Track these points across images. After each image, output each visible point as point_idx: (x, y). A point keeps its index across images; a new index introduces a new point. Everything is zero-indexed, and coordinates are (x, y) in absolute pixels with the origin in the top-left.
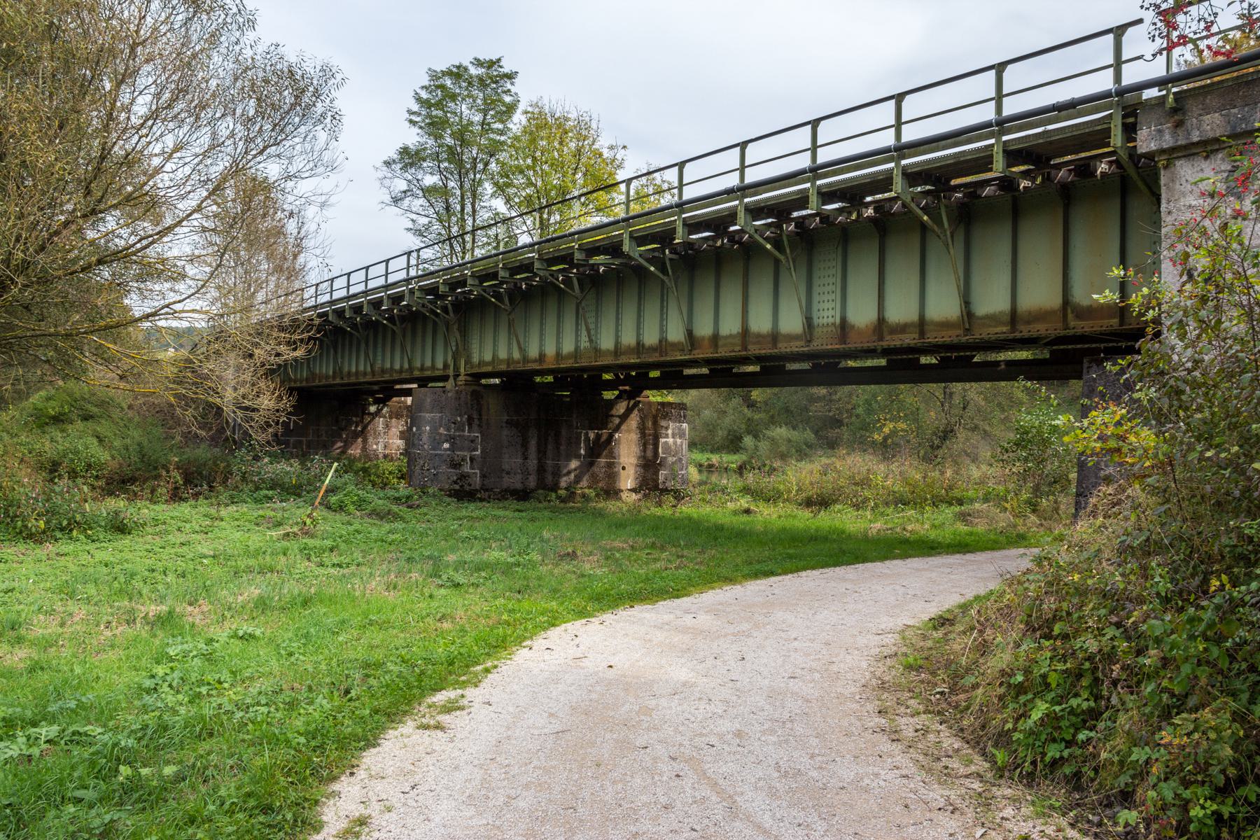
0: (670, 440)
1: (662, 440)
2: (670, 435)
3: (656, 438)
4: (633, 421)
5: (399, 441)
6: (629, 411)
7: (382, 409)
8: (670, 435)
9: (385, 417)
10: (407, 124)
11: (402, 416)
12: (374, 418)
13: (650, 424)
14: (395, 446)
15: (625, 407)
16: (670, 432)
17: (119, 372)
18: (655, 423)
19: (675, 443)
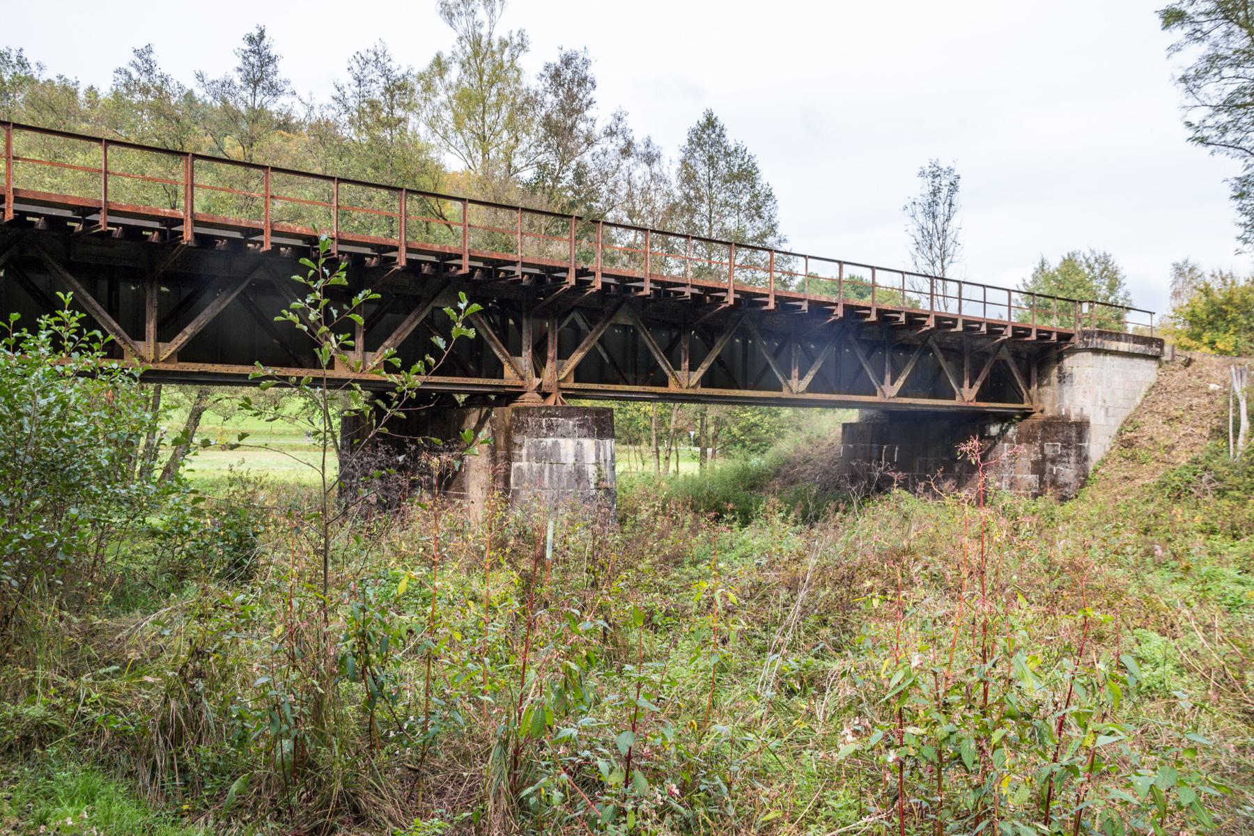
0: (524, 464)
1: (515, 465)
2: (524, 458)
3: (509, 459)
4: (484, 433)
5: (1031, 476)
6: (481, 423)
7: (1007, 430)
8: (524, 458)
9: (1011, 441)
10: (598, 84)
11: (1035, 439)
12: (995, 443)
13: (501, 441)
14: (1024, 484)
15: (477, 418)
16: (524, 451)
17: (813, 702)
18: (508, 439)
19: (530, 469)
